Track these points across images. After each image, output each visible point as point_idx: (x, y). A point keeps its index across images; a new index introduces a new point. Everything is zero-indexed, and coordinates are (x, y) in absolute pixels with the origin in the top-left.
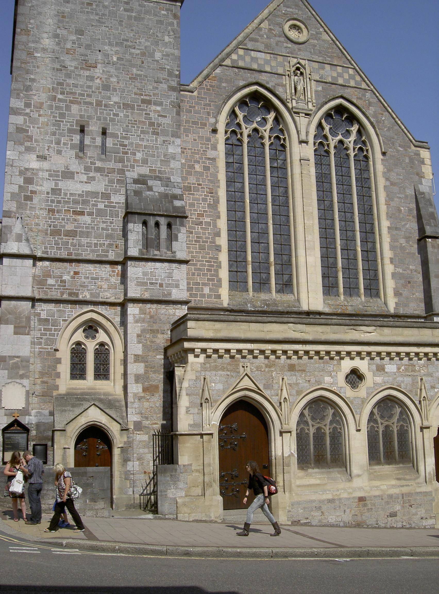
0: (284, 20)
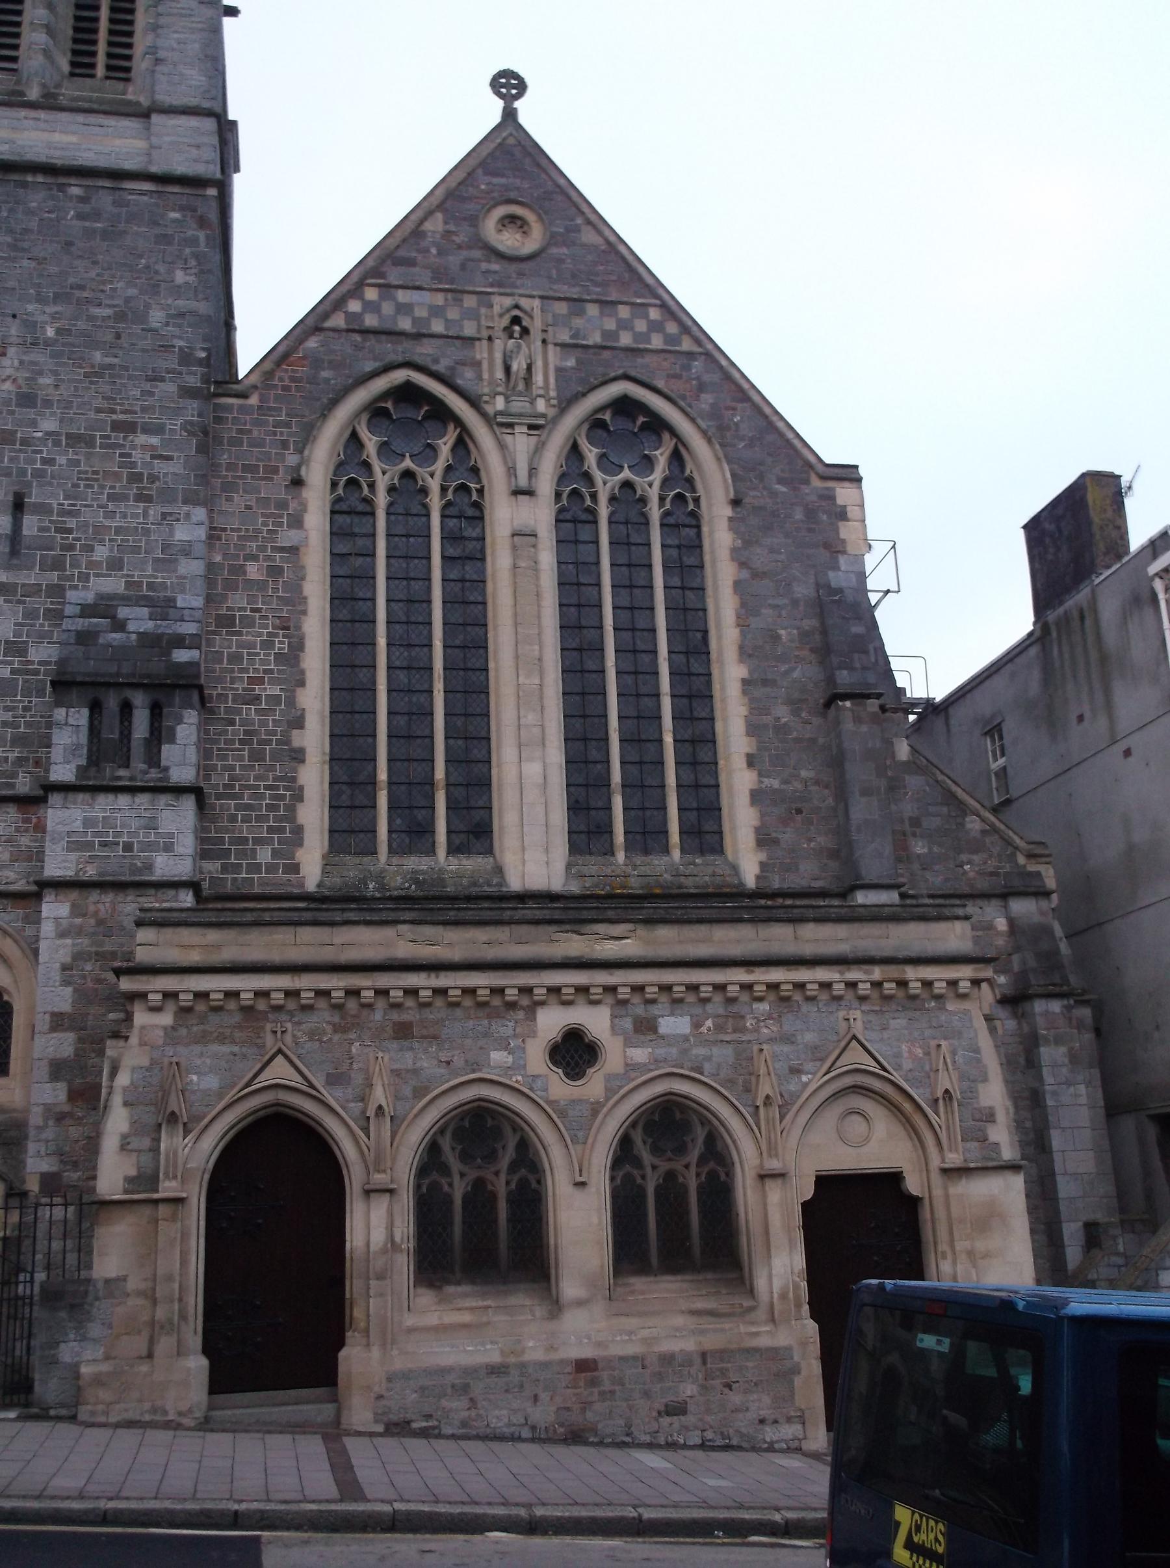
0: (484, 205)
